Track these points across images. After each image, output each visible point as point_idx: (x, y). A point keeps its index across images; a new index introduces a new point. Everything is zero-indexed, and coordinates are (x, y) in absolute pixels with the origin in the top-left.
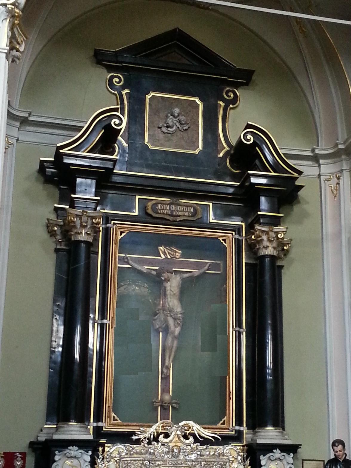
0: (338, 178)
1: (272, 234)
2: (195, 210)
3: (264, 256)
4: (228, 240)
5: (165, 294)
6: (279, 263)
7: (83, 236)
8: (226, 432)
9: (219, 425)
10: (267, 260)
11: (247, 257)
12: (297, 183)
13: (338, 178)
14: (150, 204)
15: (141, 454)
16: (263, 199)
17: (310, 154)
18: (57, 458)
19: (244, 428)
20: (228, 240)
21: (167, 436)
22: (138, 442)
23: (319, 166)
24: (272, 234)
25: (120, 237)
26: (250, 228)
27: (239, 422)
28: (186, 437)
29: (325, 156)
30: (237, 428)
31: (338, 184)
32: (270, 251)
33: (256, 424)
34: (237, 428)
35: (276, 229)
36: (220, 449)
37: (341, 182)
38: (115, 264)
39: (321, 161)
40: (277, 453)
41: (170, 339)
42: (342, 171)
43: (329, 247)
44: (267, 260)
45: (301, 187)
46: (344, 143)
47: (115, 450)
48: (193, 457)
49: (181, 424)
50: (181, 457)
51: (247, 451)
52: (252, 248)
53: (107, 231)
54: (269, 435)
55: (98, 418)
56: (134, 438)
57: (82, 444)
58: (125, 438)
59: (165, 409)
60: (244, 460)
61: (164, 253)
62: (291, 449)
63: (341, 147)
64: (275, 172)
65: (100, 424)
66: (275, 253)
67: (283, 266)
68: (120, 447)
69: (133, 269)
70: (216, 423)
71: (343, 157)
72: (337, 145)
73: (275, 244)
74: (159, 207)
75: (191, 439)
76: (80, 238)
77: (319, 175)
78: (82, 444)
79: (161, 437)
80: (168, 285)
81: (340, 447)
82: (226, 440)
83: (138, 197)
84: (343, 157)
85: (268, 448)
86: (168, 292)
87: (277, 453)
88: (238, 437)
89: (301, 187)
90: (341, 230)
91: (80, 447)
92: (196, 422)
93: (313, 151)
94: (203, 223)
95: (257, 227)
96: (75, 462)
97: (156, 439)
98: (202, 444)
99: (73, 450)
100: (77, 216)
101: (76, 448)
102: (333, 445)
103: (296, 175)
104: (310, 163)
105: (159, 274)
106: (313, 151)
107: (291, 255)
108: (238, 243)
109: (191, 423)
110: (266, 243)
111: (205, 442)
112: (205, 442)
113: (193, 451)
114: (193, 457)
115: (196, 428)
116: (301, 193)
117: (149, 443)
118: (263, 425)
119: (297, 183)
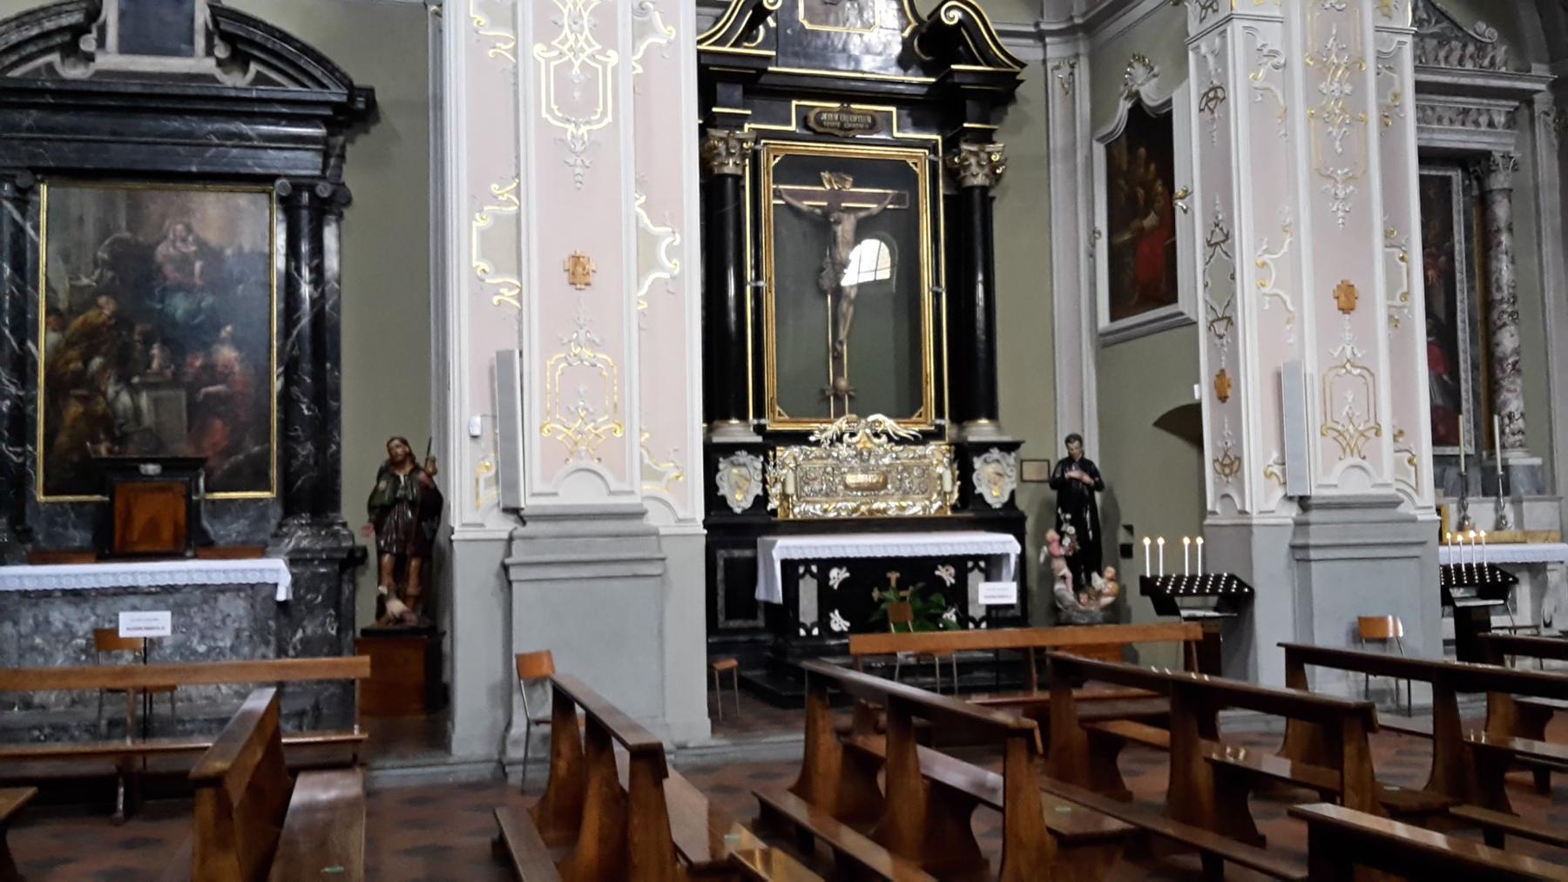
0: (1072, 66)
1: (983, 156)
2: (874, 120)
3: (973, 188)
4: (919, 160)
5: (835, 241)
6: (991, 194)
7: (730, 168)
8: (924, 427)
9: (914, 419)
10: (977, 192)
11: (946, 186)
12: (1018, 77)
13: (1072, 66)
14: (812, 115)
15: (821, 458)
16: (968, 103)
17: (1032, 29)
18: (721, 466)
19: (946, 422)
20: (919, 160)
21: (853, 435)
22: (817, 443)
23: (1045, 46)
24: (983, 156)
25: (773, 163)
26: (951, 145)
27: (940, 414)
28: (877, 435)
29: (1052, 33)
30: (938, 422)
31: (1072, 74)
32: (980, 180)
33: (963, 415)
34: (938, 422)
35: (990, 148)
36: (920, 450)
37: (1076, 71)
38: (769, 202)
39: (1048, 40)
40: (995, 453)
41: (844, 305)
42: (1077, 56)
43: (1058, 169)
44: (977, 192)
45: (1021, 81)
46: (1083, 15)
47: (785, 453)
48: (887, 460)
49: (871, 418)
50: (872, 462)
51: (956, 453)
52: (954, 175)
53: (755, 157)
54: (982, 430)
55: (759, 413)
56: (812, 439)
57: (751, 448)
58: (801, 438)
59: (839, 399)
60: (951, 462)
61: (830, 182)
62: (1008, 447)
63: (1078, 21)
64: (989, 65)
65: (763, 421)
66: (987, 183)
67: (1158, 424)
68: (796, 450)
69: (789, 206)
70: (912, 414)
71: (1080, 35)
72: (1071, 18)
73: (987, 170)
74: (824, 116)
75: (884, 438)
76: (727, 170)
77: (1044, 62)
78: (751, 448)
79: (846, 436)
80: (839, 229)
81: (1076, 443)
82: (925, 438)
83: (794, 103)
84: (1080, 35)
85: (983, 448)
86: (840, 239)
87: (995, 453)
88: (938, 434)
89: (1021, 81)
90: (1074, 143)
91: (750, 452)
92: (889, 416)
93: (1037, 25)
94: (1383, 641)
95: (965, 147)
96: (744, 471)
97: (840, 439)
98: (898, 443)
99: (742, 456)
100: (721, 139)
101: (744, 453)
102: (1068, 441)
103: (1017, 69)
104: (1031, 41)
105: (826, 213)
106: (1037, 25)
107: (1005, 181)
108: (934, 165)
109: (880, 417)
110: (974, 169)
111: (902, 441)
112: (902, 441)
113: (886, 452)
114: (887, 460)
115: (889, 424)
116: (1020, 90)
117: (832, 443)
118: (974, 417)
119: (1018, 77)
